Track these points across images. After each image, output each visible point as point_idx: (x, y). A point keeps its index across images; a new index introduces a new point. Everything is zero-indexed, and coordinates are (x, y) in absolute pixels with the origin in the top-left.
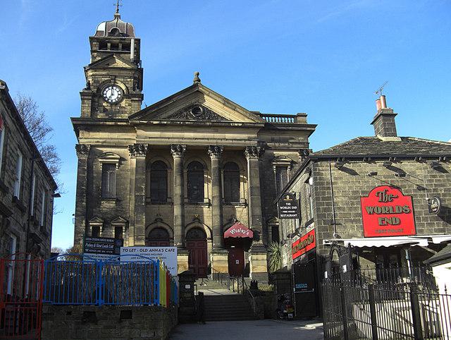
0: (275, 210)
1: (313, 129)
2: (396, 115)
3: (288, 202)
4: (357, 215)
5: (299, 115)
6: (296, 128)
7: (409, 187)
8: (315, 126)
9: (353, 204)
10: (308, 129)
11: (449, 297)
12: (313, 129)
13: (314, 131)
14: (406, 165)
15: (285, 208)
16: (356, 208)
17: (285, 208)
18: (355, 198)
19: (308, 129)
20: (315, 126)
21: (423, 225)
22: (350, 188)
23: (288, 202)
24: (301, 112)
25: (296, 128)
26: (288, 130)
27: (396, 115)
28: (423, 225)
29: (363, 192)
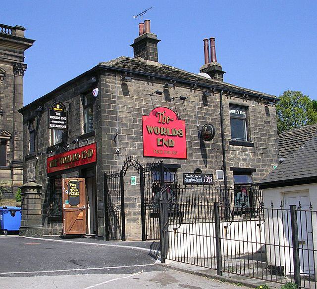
0: (90, 117)
1: (31, 44)
2: (159, 41)
3: (58, 111)
4: (138, 133)
5: (16, 28)
6: (14, 41)
7: (184, 112)
8: (32, 41)
9: (135, 121)
10: (26, 43)
11: (314, 216)
12: (31, 44)
13: (31, 46)
14: (183, 90)
15: (55, 117)
16: (137, 126)
17: (55, 117)
18: (137, 116)
19: (26, 43)
20: (32, 41)
21: (192, 150)
22: (134, 104)
23: (58, 111)
24: (20, 25)
25: (14, 41)
26: (7, 41)
27: (159, 41)
28: (192, 150)
29: (145, 111)
